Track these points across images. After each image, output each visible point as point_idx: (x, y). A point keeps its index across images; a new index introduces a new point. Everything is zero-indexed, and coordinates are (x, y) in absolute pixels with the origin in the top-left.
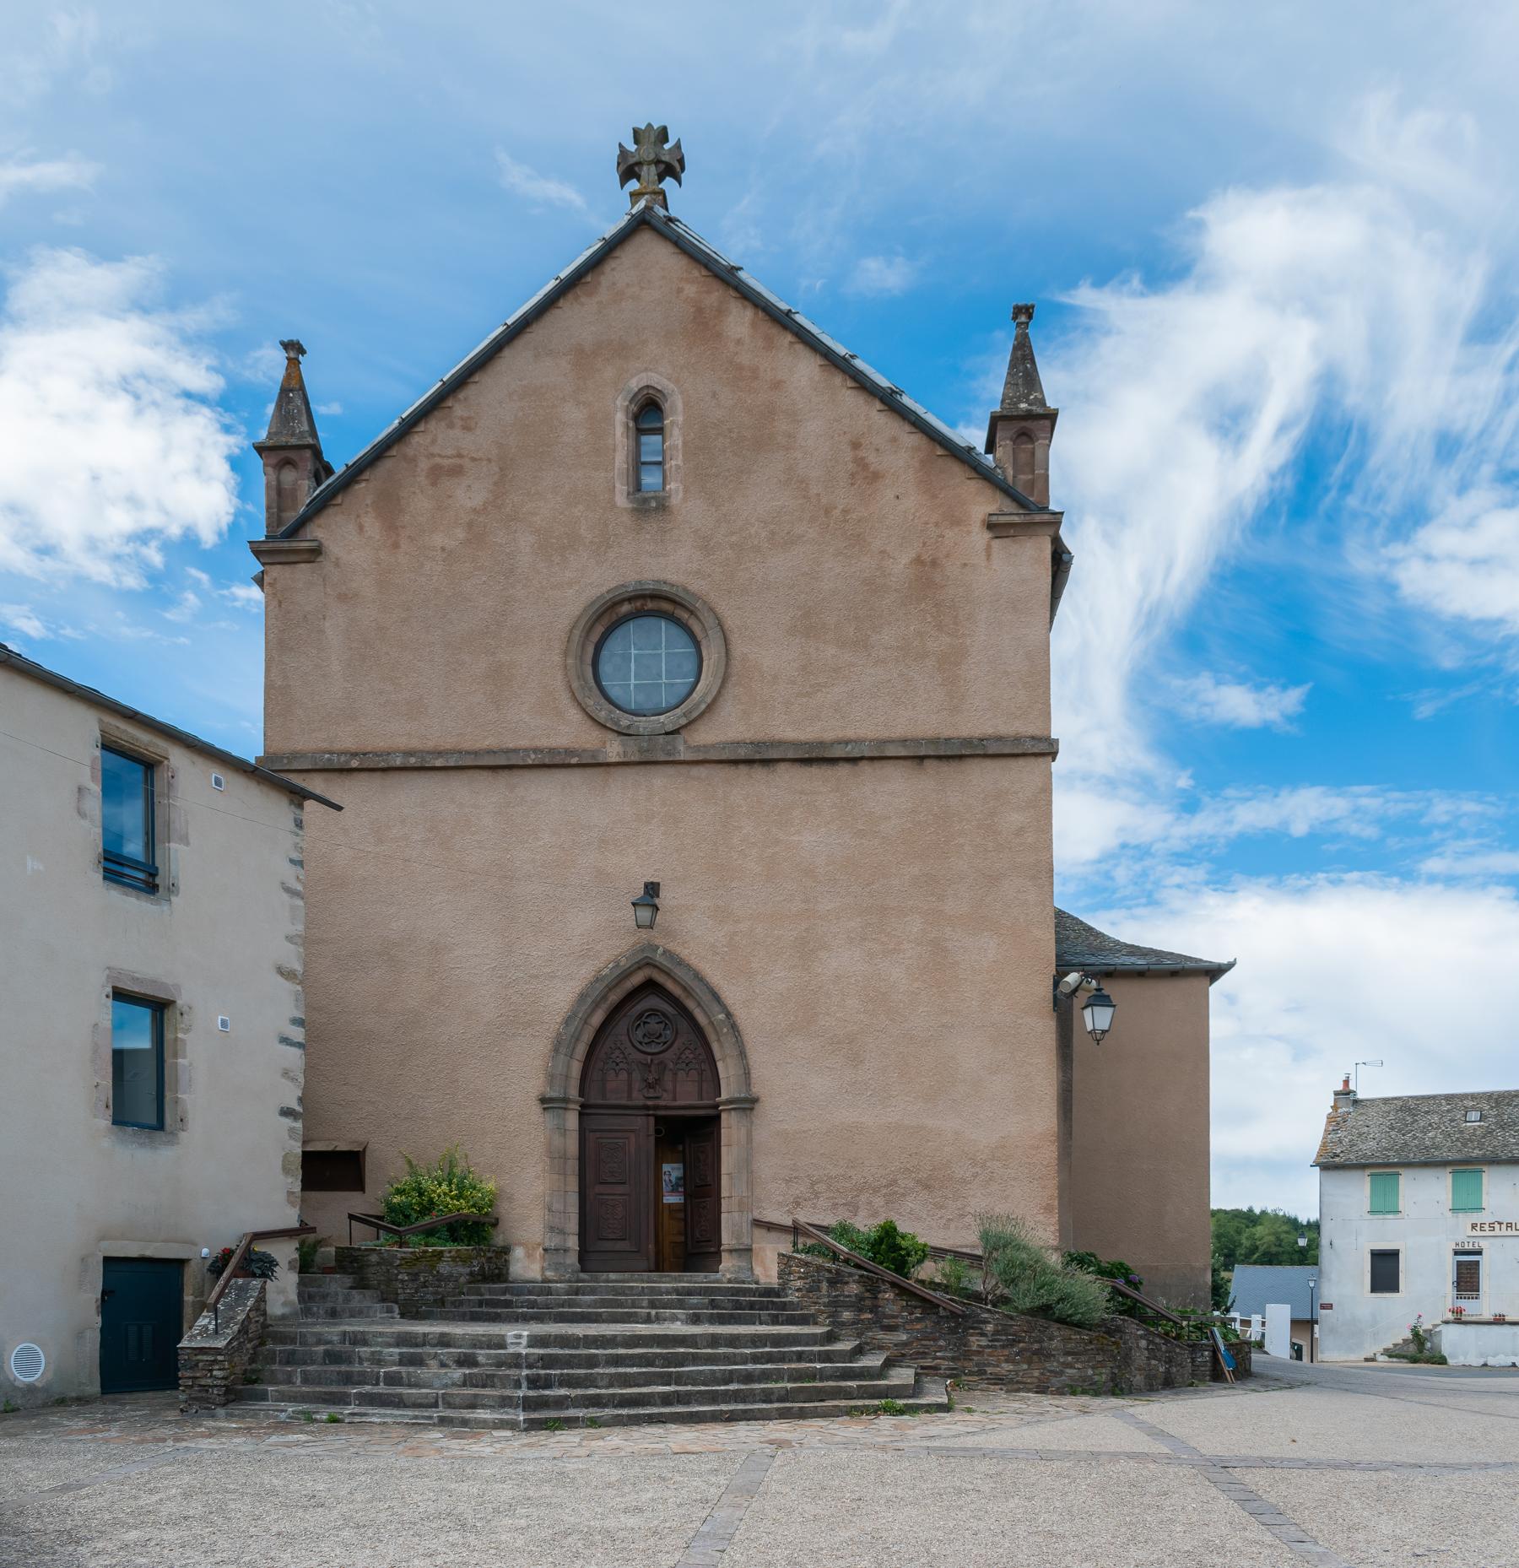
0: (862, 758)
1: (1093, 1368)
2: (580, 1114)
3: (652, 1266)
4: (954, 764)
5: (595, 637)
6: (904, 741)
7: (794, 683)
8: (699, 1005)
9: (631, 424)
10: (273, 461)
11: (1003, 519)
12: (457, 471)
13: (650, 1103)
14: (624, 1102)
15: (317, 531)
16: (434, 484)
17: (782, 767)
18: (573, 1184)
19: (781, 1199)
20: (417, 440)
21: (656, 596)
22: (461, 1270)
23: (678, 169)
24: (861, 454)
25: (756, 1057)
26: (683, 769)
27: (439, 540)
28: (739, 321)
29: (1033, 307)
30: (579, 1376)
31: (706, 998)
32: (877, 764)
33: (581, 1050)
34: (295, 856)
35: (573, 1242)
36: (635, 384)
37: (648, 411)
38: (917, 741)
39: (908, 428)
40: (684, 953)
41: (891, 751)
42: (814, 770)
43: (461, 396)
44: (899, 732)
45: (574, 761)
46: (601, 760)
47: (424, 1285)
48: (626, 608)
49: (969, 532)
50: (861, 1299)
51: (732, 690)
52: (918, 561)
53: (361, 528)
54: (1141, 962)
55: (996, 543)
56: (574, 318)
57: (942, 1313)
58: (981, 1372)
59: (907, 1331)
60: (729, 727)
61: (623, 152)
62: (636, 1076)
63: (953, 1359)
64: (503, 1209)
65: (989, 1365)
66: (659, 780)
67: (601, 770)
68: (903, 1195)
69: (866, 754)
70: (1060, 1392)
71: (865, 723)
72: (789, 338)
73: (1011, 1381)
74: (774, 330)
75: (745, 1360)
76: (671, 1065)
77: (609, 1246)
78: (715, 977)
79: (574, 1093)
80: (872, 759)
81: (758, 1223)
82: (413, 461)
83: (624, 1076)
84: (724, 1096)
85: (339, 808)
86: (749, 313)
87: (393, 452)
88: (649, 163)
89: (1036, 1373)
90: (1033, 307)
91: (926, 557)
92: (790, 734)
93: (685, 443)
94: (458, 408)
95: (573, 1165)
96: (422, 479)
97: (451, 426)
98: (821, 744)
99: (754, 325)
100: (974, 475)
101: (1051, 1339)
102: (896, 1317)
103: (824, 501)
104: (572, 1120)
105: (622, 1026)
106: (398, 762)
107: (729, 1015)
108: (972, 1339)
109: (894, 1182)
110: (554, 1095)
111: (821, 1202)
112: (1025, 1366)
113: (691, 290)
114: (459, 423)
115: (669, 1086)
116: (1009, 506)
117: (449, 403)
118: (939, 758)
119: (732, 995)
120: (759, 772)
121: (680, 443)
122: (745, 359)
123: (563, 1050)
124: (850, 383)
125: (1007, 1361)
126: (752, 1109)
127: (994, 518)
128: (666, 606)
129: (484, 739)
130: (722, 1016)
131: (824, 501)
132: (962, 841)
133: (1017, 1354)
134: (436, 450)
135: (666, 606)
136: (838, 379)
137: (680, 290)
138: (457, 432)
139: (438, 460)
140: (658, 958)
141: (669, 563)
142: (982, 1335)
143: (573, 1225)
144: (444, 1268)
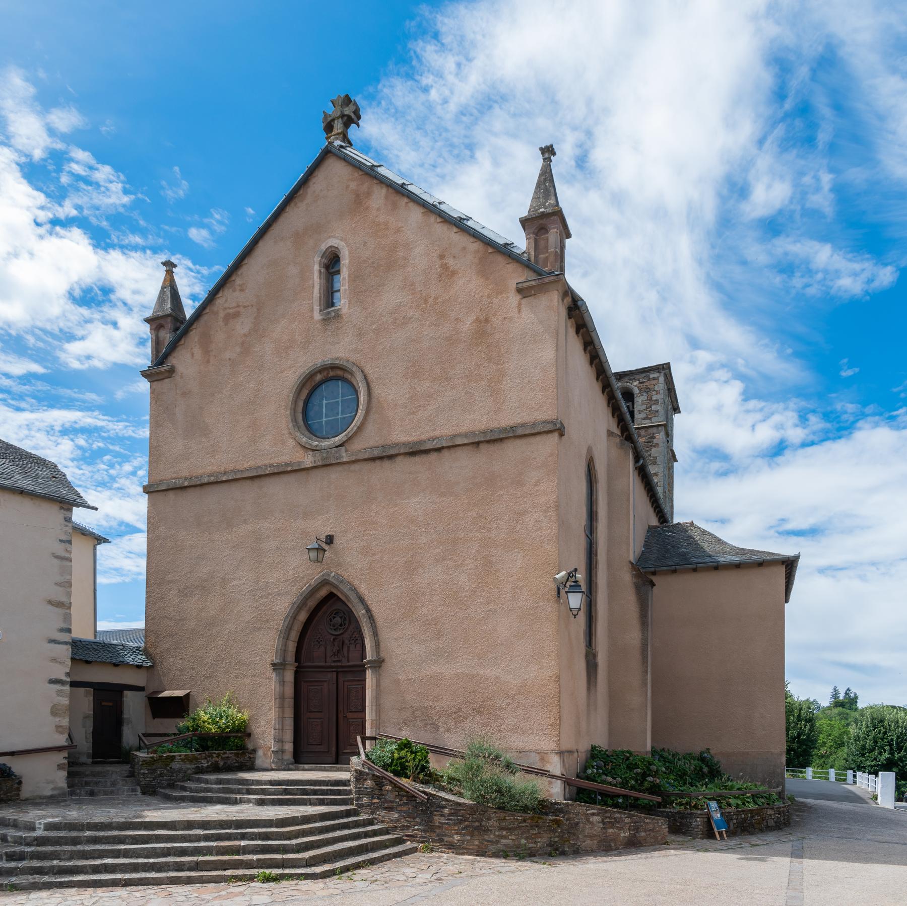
0: (443, 448)
1: (526, 838)
4: (497, 445)
5: (304, 396)
6: (465, 435)
7: (406, 407)
9: (323, 270)
10: (154, 326)
11: (525, 285)
12: (237, 315)
14: (323, 664)
15: (173, 360)
16: (226, 324)
17: (399, 459)
18: (289, 714)
20: (219, 301)
21: (334, 367)
22: (189, 766)
23: (355, 119)
24: (445, 261)
25: (384, 634)
26: (346, 467)
27: (228, 355)
28: (379, 195)
29: (551, 146)
30: (46, 852)
32: (452, 451)
33: (295, 635)
34: (64, 538)
36: (324, 247)
37: (332, 263)
38: (474, 434)
39: (472, 240)
40: (346, 575)
41: (459, 441)
42: (417, 459)
43: (239, 273)
44: (465, 428)
45: (289, 469)
46: (303, 467)
47: (161, 775)
48: (319, 377)
49: (508, 297)
50: (373, 789)
51: (373, 416)
52: (478, 321)
53: (193, 355)
54: (737, 559)
55: (524, 301)
56: (295, 217)
57: (418, 800)
58: (441, 841)
59: (399, 812)
60: (370, 440)
61: (326, 115)
63: (422, 831)
64: (253, 727)
65: (446, 835)
66: (334, 475)
67: (304, 473)
69: (445, 445)
70: (495, 855)
71: (446, 428)
72: (406, 200)
73: (460, 848)
74: (397, 198)
75: (198, 838)
78: (363, 590)
80: (449, 447)
82: (217, 313)
83: (322, 649)
85: (96, 509)
86: (384, 191)
87: (207, 310)
88: (338, 118)
89: (476, 843)
90: (551, 146)
91: (482, 318)
92: (403, 438)
93: (349, 276)
94: (238, 280)
95: (289, 702)
96: (221, 323)
97: (234, 291)
98: (420, 442)
99: (386, 198)
100: (510, 261)
101: (489, 819)
102: (392, 802)
103: (424, 294)
106: (206, 480)
107: (368, 611)
108: (436, 818)
109: (459, 710)
111: (418, 723)
112: (469, 838)
113: (353, 185)
114: (238, 288)
115: (346, 654)
116: (531, 276)
117: (233, 278)
118: (488, 442)
120: (387, 464)
121: (346, 276)
122: (382, 218)
124: (439, 220)
125: (457, 834)
126: (380, 667)
127: (520, 285)
128: (339, 373)
129: (247, 463)
130: (363, 611)
131: (424, 294)
132: (502, 493)
133: (463, 829)
134: (227, 305)
135: (339, 373)
136: (433, 219)
137: (347, 187)
138: (237, 293)
139: (228, 311)
141: (340, 349)
142: (442, 815)
143: (289, 736)
144: (175, 765)
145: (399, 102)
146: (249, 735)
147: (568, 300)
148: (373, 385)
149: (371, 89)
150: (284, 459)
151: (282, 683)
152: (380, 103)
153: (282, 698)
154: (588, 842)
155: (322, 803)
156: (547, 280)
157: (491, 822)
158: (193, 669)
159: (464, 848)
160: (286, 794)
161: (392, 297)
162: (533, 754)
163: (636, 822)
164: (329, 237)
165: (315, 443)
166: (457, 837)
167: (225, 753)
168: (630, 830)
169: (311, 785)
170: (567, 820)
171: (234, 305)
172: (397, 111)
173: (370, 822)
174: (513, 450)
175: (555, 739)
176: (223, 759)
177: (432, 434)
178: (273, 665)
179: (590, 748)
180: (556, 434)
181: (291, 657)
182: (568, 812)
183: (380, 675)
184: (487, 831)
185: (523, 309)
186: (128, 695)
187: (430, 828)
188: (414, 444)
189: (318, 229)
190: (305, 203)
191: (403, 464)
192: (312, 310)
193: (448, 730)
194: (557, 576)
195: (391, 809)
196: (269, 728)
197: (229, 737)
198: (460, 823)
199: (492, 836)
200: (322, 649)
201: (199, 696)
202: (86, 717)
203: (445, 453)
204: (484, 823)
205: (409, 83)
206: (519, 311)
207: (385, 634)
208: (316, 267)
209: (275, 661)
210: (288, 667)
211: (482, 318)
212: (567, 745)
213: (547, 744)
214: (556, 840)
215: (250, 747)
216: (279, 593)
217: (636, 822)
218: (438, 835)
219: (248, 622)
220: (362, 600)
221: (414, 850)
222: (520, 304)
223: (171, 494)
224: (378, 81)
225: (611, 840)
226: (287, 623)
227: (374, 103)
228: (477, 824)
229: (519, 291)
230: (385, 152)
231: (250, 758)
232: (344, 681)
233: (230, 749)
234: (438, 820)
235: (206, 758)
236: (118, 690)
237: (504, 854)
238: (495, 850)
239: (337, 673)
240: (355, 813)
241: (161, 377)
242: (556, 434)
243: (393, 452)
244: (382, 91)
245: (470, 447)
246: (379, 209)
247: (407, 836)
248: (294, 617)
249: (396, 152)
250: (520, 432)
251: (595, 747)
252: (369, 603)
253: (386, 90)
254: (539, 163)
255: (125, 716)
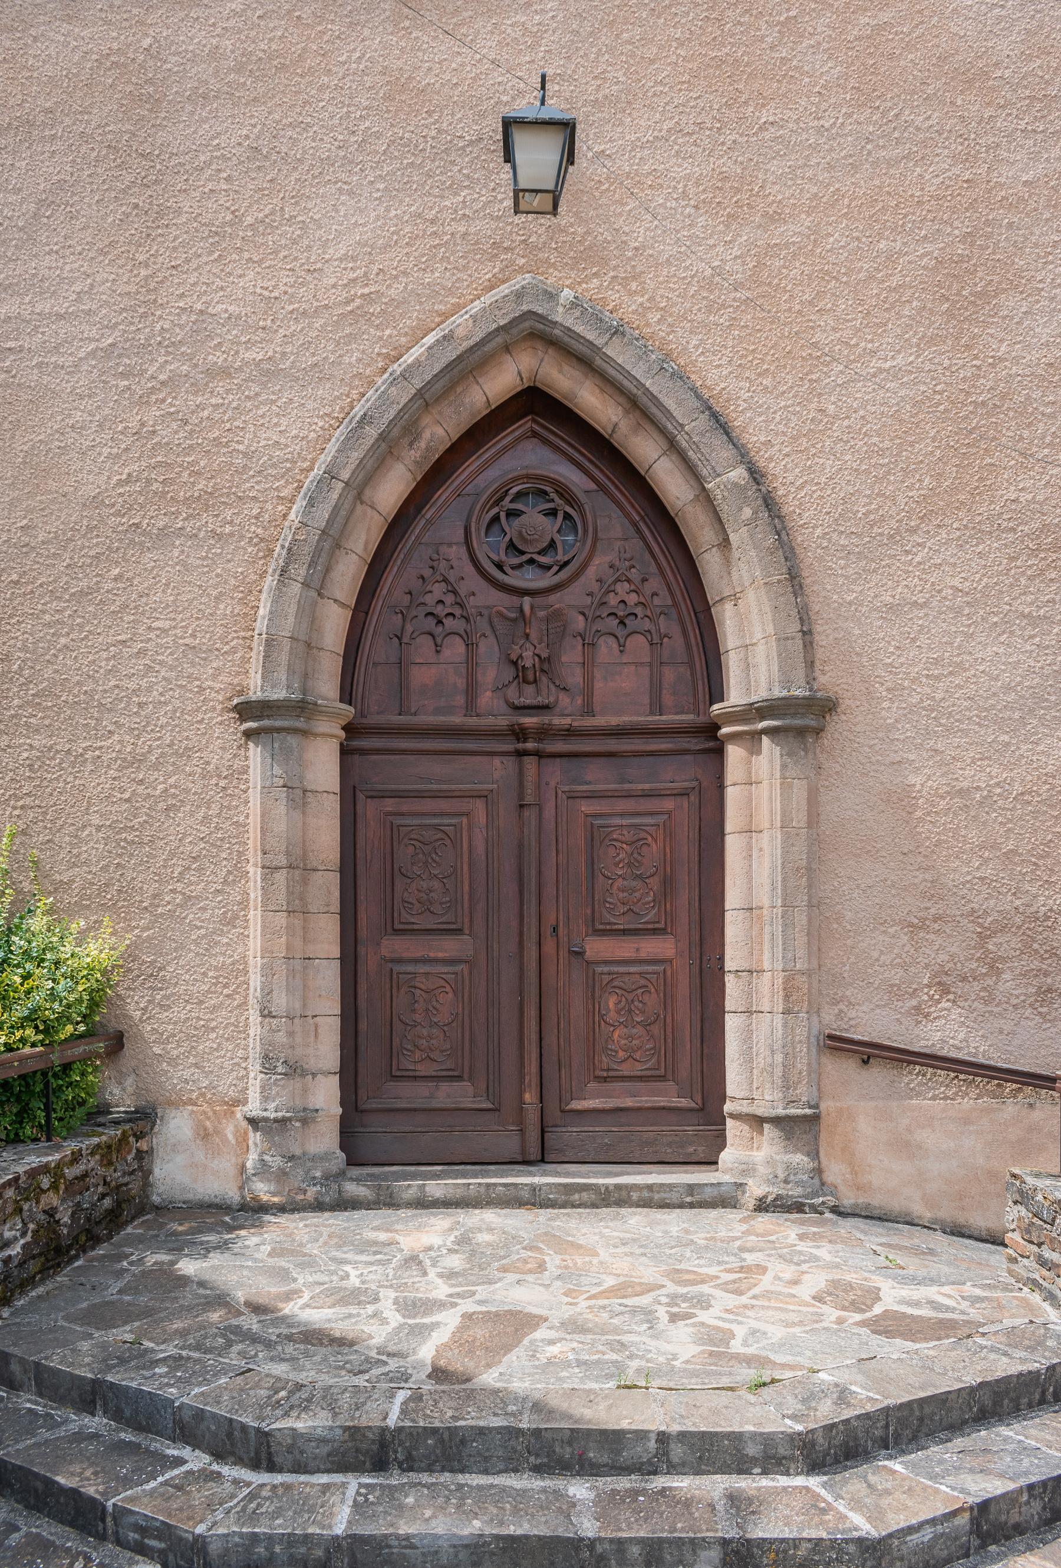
2: (345, 752)
3: (534, 1152)
8: (673, 446)
13: (529, 721)
18: (327, 938)
19: (896, 976)
25: (832, 585)
31: (692, 426)
33: (348, 574)
35: (326, 1095)
62: (488, 649)
76: (580, 623)
77: (414, 1094)
78: (718, 374)
79: (327, 686)
81: (837, 1044)
83: (455, 649)
84: (736, 696)
95: (326, 888)
104: (323, 765)
105: (445, 522)
107: (756, 475)
110: (279, 694)
111: (1007, 983)
115: (574, 677)
119: (765, 421)
123: (299, 571)
126: (818, 731)
130: (738, 474)
140: (559, 315)
143: (326, 1050)
151: (298, 794)
153: (299, 866)
178: (245, 710)
200: (455, 649)
209: (256, 688)
216: (268, 372)
219: (96, 501)
248: (359, 489)
252: (753, 438)
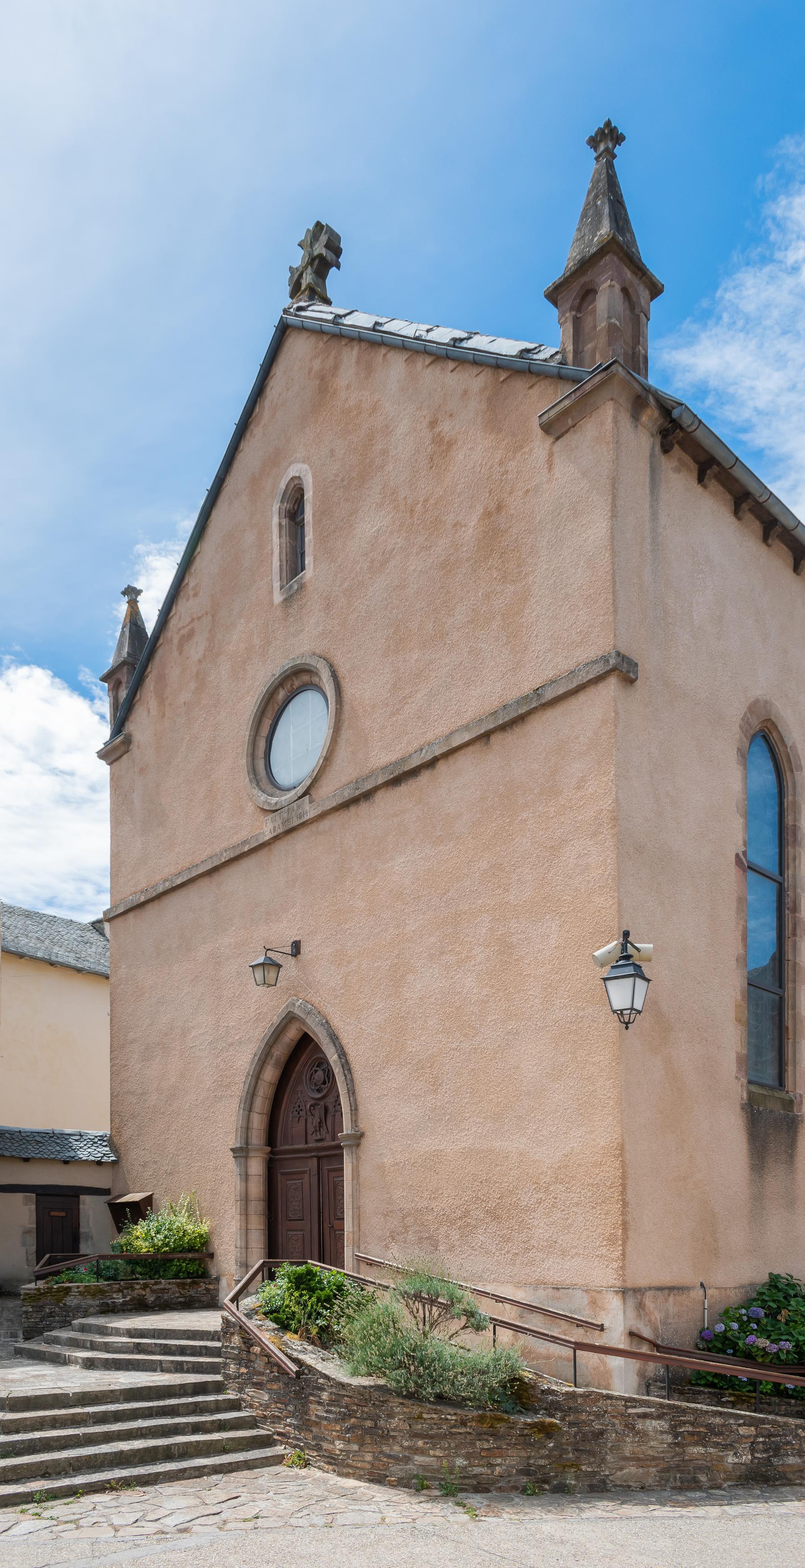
1: (468, 1456)
4: (518, 730)
6: (466, 727)
7: (387, 705)
9: (284, 522)
14: (301, 1146)
17: (380, 795)
22: (90, 1302)
24: (437, 430)
26: (313, 827)
29: (608, 124)
32: (451, 760)
33: (261, 1104)
39: (475, 370)
41: (456, 742)
46: (261, 841)
48: (282, 694)
49: (531, 450)
52: (487, 514)
59: (270, 1391)
63: (296, 1427)
65: (324, 1439)
66: (300, 843)
68: (476, 1227)
70: (403, 1483)
87: (161, 641)
89: (369, 1457)
90: (608, 124)
94: (190, 582)
95: (257, 1207)
96: (175, 653)
97: (187, 600)
100: (534, 379)
101: (391, 1416)
102: (262, 1374)
106: (161, 889)
108: (312, 1406)
109: (466, 1214)
111: (411, 1237)
112: (355, 1447)
114: (191, 593)
117: (186, 581)
120: (363, 808)
124: (428, 360)
125: (339, 1438)
127: (545, 417)
132: (525, 815)
133: (348, 1430)
142: (319, 1403)
145: (750, 308)
146: (212, 1256)
147: (651, 416)
148: (346, 684)
149: (705, 303)
150: (244, 834)
151: (246, 1177)
152: (720, 318)
154: (632, 1469)
155: (179, 1368)
156: (588, 387)
157: (395, 1422)
158: (155, 1162)
159: (348, 1466)
160: (139, 1352)
161: (372, 523)
162: (579, 1293)
163: (770, 1436)
164: (290, 464)
165: (274, 800)
166: (339, 1445)
167: (156, 1284)
168: (753, 1450)
169: (188, 1338)
170: (571, 1425)
171: (189, 619)
172: (748, 320)
173: (235, 1405)
174: (543, 731)
175: (615, 1265)
176: (152, 1291)
177: (422, 741)
179: (765, 1278)
180: (612, 682)
181: (257, 1137)
182: (577, 1411)
183: (358, 1159)
184: (386, 1437)
185: (557, 460)
186: (87, 1201)
187: (305, 1425)
188: (396, 764)
189: (275, 460)
190: (261, 425)
191: (385, 801)
192: (271, 592)
193: (451, 1248)
194: (596, 954)
195: (259, 1386)
196: (234, 1245)
197: (172, 1260)
198: (343, 1419)
199: (397, 1448)
201: (163, 1202)
202: (27, 1232)
203: (441, 766)
204: (382, 1423)
205: (767, 269)
206: (550, 469)
207: (364, 1091)
208: (275, 520)
210: (252, 1154)
211: (492, 506)
212: (648, 1273)
213: (604, 1275)
214: (542, 1462)
215: (214, 1273)
217: (770, 1436)
218: (314, 1438)
219: (209, 1090)
220: (334, 1038)
221: (278, 1460)
222: (551, 455)
223: (131, 916)
224: (715, 286)
225: (700, 1469)
226: (247, 1086)
227: (710, 323)
228: (369, 1424)
229: (547, 428)
230: (731, 390)
231: (208, 1290)
232: (329, 1171)
233: (185, 1273)
234: (316, 1411)
235: (119, 1291)
236: (74, 1193)
237: (416, 1484)
238: (401, 1474)
239: (319, 1158)
240: (219, 1388)
241: (118, 754)
242: (612, 682)
243: (368, 786)
244: (722, 298)
245: (477, 747)
246: (348, 387)
247: (279, 1434)
248: (257, 1076)
249: (748, 383)
250: (549, 695)
251: (778, 1276)
253: (728, 296)
254: (588, 165)
255: (82, 1230)
